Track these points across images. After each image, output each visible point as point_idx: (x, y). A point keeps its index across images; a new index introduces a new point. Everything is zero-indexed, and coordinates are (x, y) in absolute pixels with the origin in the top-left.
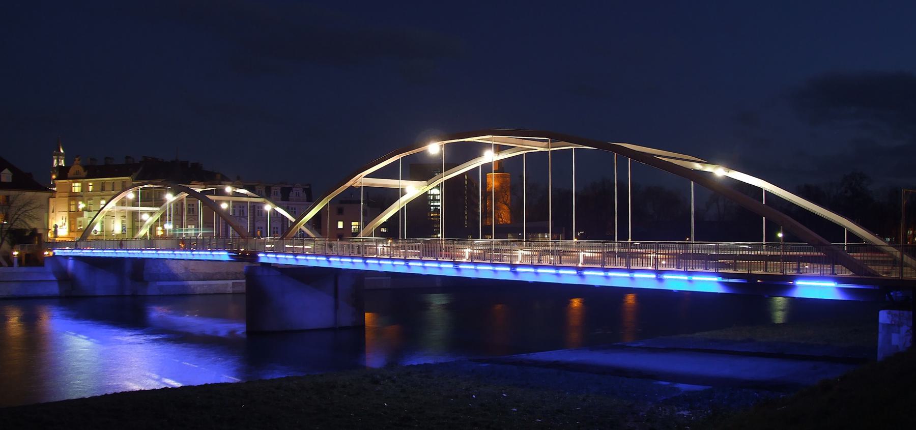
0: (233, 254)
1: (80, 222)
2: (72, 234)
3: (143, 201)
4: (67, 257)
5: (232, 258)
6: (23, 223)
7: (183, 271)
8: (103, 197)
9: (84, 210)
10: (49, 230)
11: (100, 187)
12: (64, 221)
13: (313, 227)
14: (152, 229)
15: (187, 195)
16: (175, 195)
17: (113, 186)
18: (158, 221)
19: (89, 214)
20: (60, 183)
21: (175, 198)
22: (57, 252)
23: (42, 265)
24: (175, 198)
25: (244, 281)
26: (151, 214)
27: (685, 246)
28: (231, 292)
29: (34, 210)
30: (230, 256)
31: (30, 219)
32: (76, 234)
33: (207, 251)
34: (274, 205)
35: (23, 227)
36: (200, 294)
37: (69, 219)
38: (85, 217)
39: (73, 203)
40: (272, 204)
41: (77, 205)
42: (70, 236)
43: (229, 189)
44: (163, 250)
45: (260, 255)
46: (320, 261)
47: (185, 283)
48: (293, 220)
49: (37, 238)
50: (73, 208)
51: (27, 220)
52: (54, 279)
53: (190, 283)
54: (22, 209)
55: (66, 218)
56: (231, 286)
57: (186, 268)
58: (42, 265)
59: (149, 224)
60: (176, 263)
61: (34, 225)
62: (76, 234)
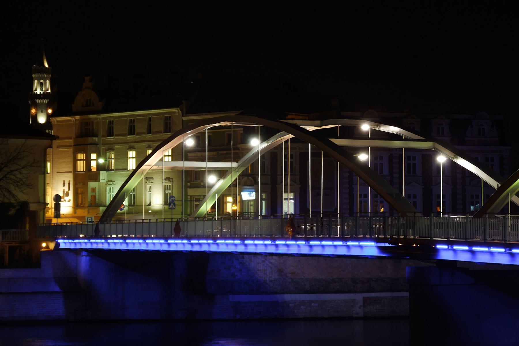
0: (387, 245)
1: (93, 190)
2: (81, 212)
3: (77, 145)
4: (77, 252)
5: (384, 253)
6: (6, 194)
7: (275, 276)
8: (132, 145)
9: (100, 168)
10: (46, 204)
11: (146, 126)
12: (66, 189)
13: (56, 175)
14: (221, 203)
15: (291, 136)
16: (264, 138)
17: (150, 126)
18: (234, 184)
19: (108, 175)
20: (58, 121)
21: (265, 145)
22: (63, 243)
23: (38, 265)
24: (265, 145)
25: (406, 294)
26: (222, 173)
27: (190, 187)
28: (361, 315)
29: (24, 171)
30: (380, 248)
31: (18, 186)
32: (86, 210)
33: (79, 238)
34: (451, 154)
35: (6, 201)
36: (305, 319)
37: (75, 184)
38: (101, 181)
39: (81, 156)
40: (448, 152)
41: (88, 161)
42: (76, 215)
43: (365, 127)
44: (254, 239)
45: (438, 246)
46: (496, 255)
47: (279, 297)
48: (494, 183)
49: (28, 219)
50: (81, 166)
51: (12, 188)
52: (57, 289)
53: (288, 297)
54: (5, 169)
55: (69, 184)
56: (362, 304)
57: (280, 271)
58: (38, 265)
59: (217, 192)
60: (263, 262)
61: (22, 197)
62: (86, 210)
